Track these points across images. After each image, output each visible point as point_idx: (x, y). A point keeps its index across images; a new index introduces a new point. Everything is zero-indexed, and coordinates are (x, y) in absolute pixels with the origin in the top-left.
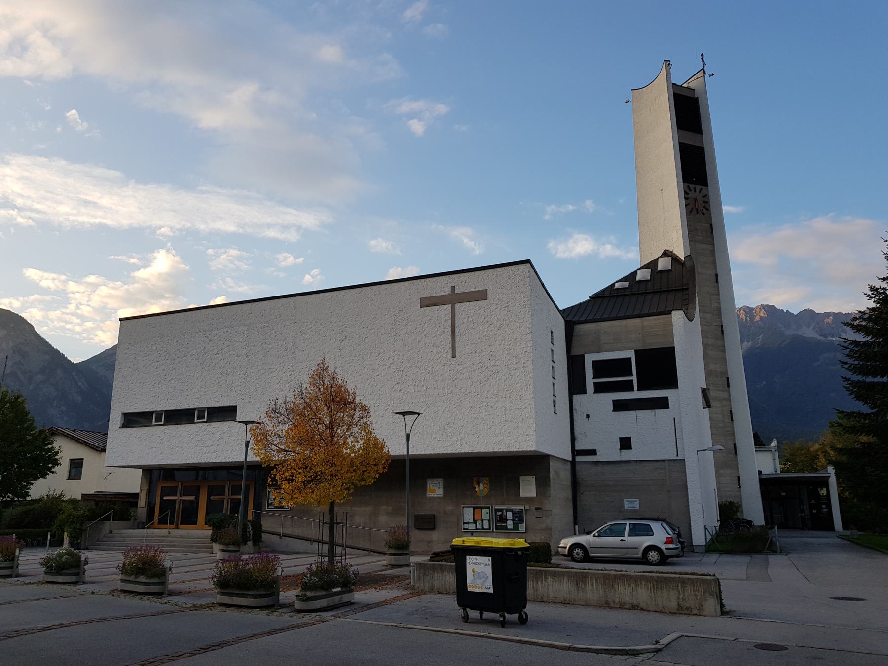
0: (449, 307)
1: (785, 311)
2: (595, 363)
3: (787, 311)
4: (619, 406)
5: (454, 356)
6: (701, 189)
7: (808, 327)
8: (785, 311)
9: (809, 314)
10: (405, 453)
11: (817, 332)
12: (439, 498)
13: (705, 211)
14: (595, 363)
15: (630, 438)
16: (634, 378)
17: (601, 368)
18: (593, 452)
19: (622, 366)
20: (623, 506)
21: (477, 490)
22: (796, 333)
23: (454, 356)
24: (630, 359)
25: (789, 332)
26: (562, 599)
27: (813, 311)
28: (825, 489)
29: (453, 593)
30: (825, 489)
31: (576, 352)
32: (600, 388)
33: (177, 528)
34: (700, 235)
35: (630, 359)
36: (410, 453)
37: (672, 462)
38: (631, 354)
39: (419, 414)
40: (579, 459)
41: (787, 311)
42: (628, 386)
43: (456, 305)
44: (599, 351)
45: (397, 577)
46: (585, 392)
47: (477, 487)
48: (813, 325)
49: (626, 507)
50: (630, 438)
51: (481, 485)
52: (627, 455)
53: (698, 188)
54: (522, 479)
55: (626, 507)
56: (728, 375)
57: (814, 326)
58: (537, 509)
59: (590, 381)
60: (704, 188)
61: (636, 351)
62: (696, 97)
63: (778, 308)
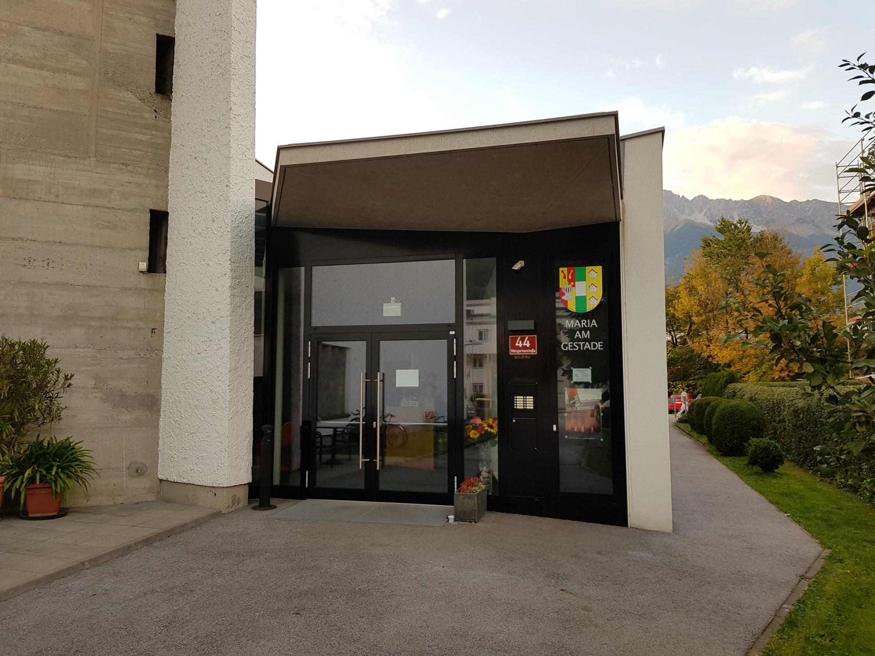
1: (681, 197)
2: (593, 348)
3: (683, 196)
7: (700, 213)
8: (681, 197)
9: (702, 199)
11: (707, 218)
14: (593, 348)
22: (689, 218)
25: (683, 218)
26: (814, 558)
27: (706, 197)
28: (595, 274)
29: (559, 381)
30: (595, 274)
37: (137, 266)
41: (683, 196)
45: (57, 487)
48: (705, 211)
57: (706, 212)
63: (675, 193)
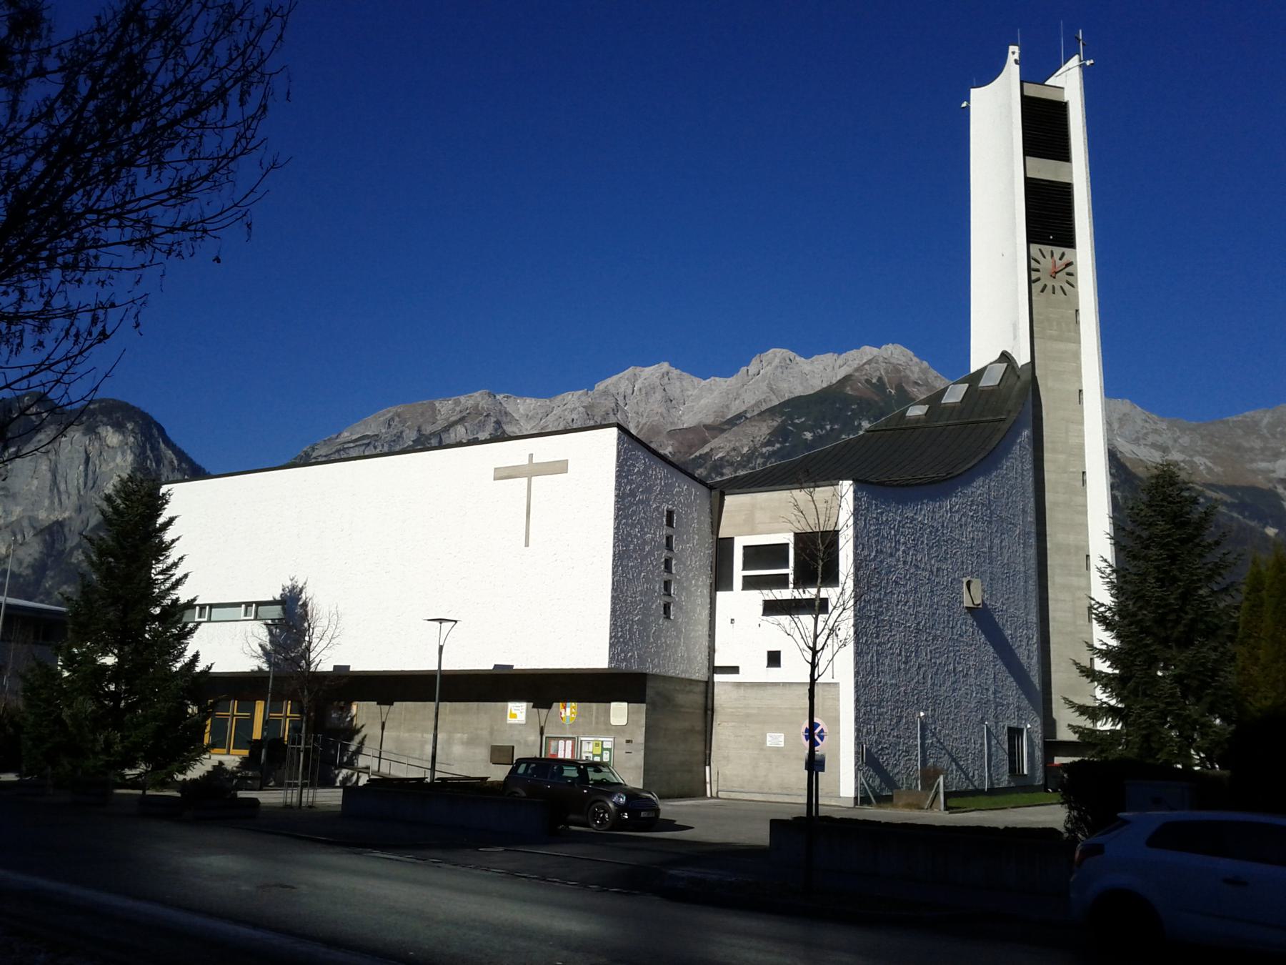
0: (525, 480)
4: (771, 608)
5: (527, 545)
6: (1063, 254)
10: (436, 668)
12: (520, 725)
13: (1067, 287)
15: (779, 652)
16: (790, 571)
17: (755, 555)
18: (734, 670)
19: (773, 554)
20: (765, 742)
21: (563, 716)
23: (527, 545)
24: (788, 544)
31: (723, 533)
32: (750, 583)
33: (228, 753)
34: (1055, 328)
35: (788, 544)
36: (442, 669)
38: (787, 538)
39: (456, 621)
40: (718, 678)
42: (781, 582)
43: (533, 478)
44: (752, 532)
46: (731, 589)
47: (563, 711)
49: (768, 744)
50: (779, 652)
51: (568, 710)
52: (774, 675)
53: (1058, 251)
54: (257, 702)
55: (768, 744)
56: (1088, 551)
58: (628, 741)
59: (739, 573)
60: (1067, 250)
61: (796, 534)
62: (1065, 101)
